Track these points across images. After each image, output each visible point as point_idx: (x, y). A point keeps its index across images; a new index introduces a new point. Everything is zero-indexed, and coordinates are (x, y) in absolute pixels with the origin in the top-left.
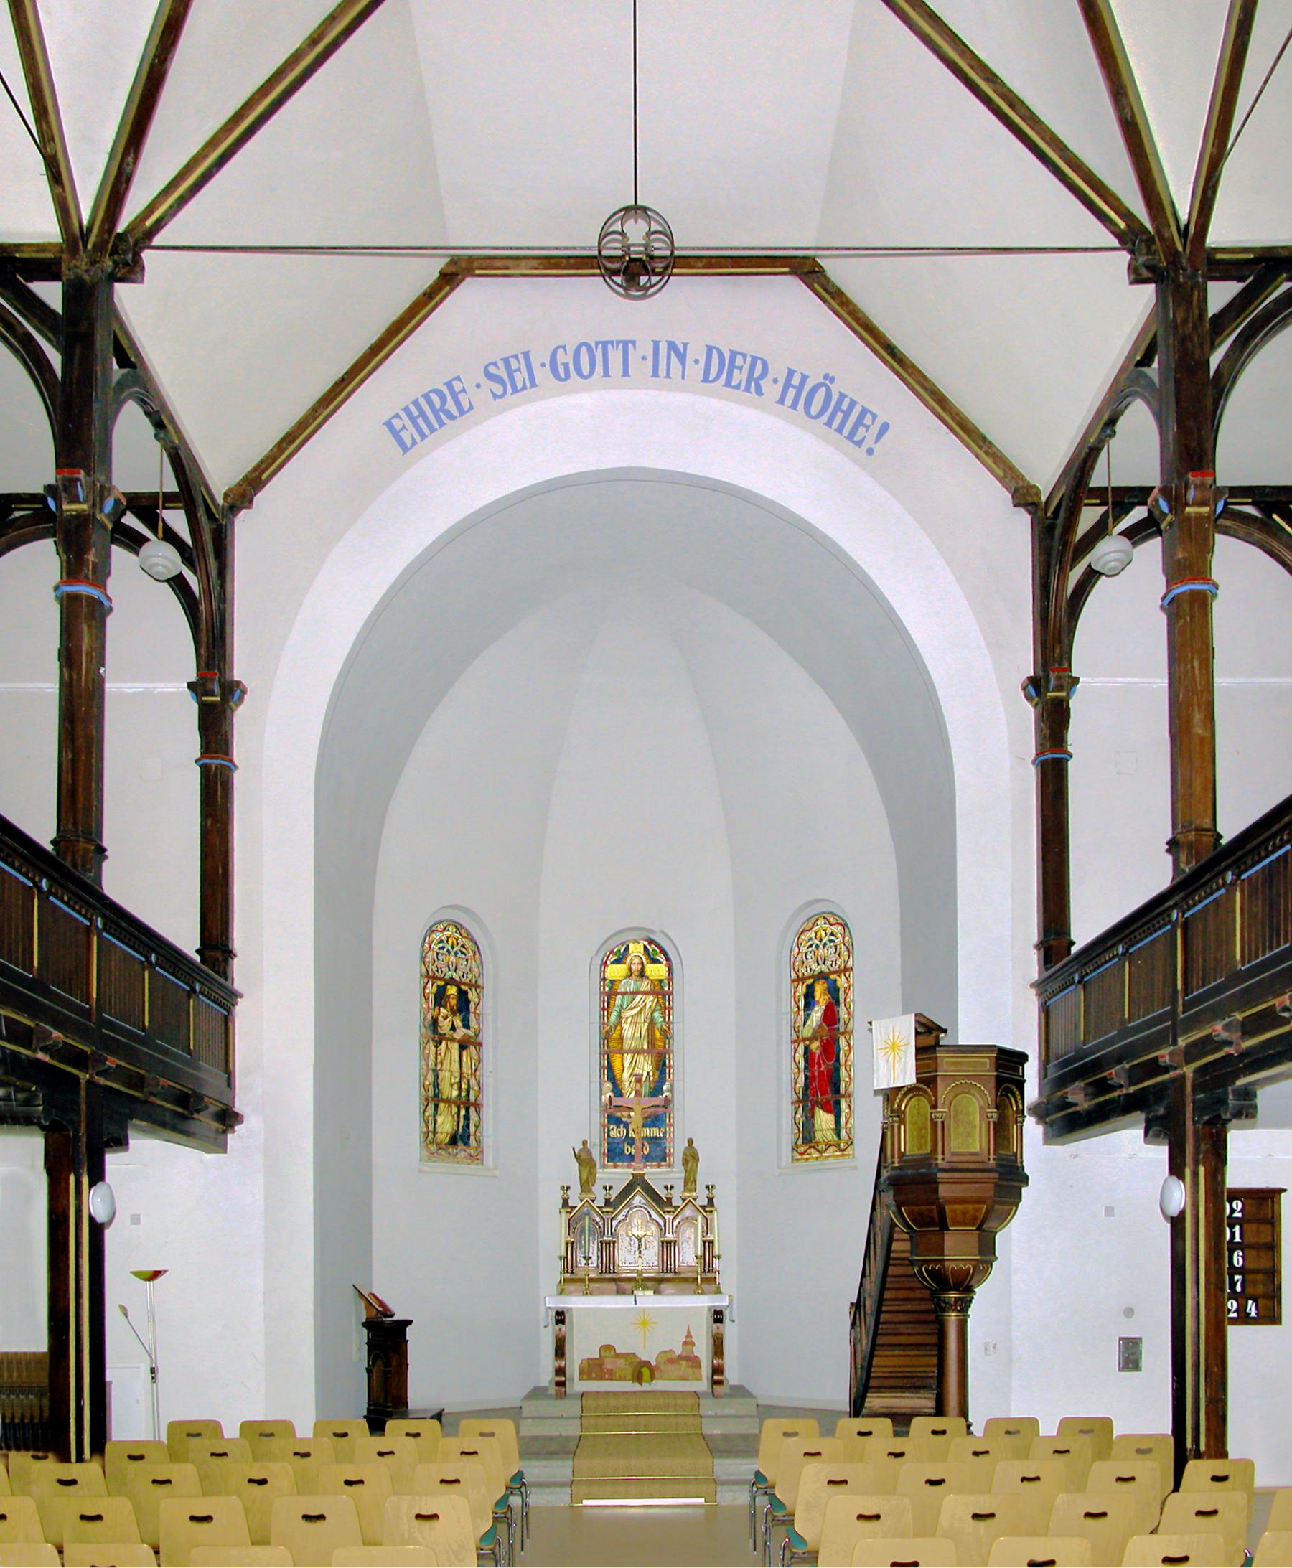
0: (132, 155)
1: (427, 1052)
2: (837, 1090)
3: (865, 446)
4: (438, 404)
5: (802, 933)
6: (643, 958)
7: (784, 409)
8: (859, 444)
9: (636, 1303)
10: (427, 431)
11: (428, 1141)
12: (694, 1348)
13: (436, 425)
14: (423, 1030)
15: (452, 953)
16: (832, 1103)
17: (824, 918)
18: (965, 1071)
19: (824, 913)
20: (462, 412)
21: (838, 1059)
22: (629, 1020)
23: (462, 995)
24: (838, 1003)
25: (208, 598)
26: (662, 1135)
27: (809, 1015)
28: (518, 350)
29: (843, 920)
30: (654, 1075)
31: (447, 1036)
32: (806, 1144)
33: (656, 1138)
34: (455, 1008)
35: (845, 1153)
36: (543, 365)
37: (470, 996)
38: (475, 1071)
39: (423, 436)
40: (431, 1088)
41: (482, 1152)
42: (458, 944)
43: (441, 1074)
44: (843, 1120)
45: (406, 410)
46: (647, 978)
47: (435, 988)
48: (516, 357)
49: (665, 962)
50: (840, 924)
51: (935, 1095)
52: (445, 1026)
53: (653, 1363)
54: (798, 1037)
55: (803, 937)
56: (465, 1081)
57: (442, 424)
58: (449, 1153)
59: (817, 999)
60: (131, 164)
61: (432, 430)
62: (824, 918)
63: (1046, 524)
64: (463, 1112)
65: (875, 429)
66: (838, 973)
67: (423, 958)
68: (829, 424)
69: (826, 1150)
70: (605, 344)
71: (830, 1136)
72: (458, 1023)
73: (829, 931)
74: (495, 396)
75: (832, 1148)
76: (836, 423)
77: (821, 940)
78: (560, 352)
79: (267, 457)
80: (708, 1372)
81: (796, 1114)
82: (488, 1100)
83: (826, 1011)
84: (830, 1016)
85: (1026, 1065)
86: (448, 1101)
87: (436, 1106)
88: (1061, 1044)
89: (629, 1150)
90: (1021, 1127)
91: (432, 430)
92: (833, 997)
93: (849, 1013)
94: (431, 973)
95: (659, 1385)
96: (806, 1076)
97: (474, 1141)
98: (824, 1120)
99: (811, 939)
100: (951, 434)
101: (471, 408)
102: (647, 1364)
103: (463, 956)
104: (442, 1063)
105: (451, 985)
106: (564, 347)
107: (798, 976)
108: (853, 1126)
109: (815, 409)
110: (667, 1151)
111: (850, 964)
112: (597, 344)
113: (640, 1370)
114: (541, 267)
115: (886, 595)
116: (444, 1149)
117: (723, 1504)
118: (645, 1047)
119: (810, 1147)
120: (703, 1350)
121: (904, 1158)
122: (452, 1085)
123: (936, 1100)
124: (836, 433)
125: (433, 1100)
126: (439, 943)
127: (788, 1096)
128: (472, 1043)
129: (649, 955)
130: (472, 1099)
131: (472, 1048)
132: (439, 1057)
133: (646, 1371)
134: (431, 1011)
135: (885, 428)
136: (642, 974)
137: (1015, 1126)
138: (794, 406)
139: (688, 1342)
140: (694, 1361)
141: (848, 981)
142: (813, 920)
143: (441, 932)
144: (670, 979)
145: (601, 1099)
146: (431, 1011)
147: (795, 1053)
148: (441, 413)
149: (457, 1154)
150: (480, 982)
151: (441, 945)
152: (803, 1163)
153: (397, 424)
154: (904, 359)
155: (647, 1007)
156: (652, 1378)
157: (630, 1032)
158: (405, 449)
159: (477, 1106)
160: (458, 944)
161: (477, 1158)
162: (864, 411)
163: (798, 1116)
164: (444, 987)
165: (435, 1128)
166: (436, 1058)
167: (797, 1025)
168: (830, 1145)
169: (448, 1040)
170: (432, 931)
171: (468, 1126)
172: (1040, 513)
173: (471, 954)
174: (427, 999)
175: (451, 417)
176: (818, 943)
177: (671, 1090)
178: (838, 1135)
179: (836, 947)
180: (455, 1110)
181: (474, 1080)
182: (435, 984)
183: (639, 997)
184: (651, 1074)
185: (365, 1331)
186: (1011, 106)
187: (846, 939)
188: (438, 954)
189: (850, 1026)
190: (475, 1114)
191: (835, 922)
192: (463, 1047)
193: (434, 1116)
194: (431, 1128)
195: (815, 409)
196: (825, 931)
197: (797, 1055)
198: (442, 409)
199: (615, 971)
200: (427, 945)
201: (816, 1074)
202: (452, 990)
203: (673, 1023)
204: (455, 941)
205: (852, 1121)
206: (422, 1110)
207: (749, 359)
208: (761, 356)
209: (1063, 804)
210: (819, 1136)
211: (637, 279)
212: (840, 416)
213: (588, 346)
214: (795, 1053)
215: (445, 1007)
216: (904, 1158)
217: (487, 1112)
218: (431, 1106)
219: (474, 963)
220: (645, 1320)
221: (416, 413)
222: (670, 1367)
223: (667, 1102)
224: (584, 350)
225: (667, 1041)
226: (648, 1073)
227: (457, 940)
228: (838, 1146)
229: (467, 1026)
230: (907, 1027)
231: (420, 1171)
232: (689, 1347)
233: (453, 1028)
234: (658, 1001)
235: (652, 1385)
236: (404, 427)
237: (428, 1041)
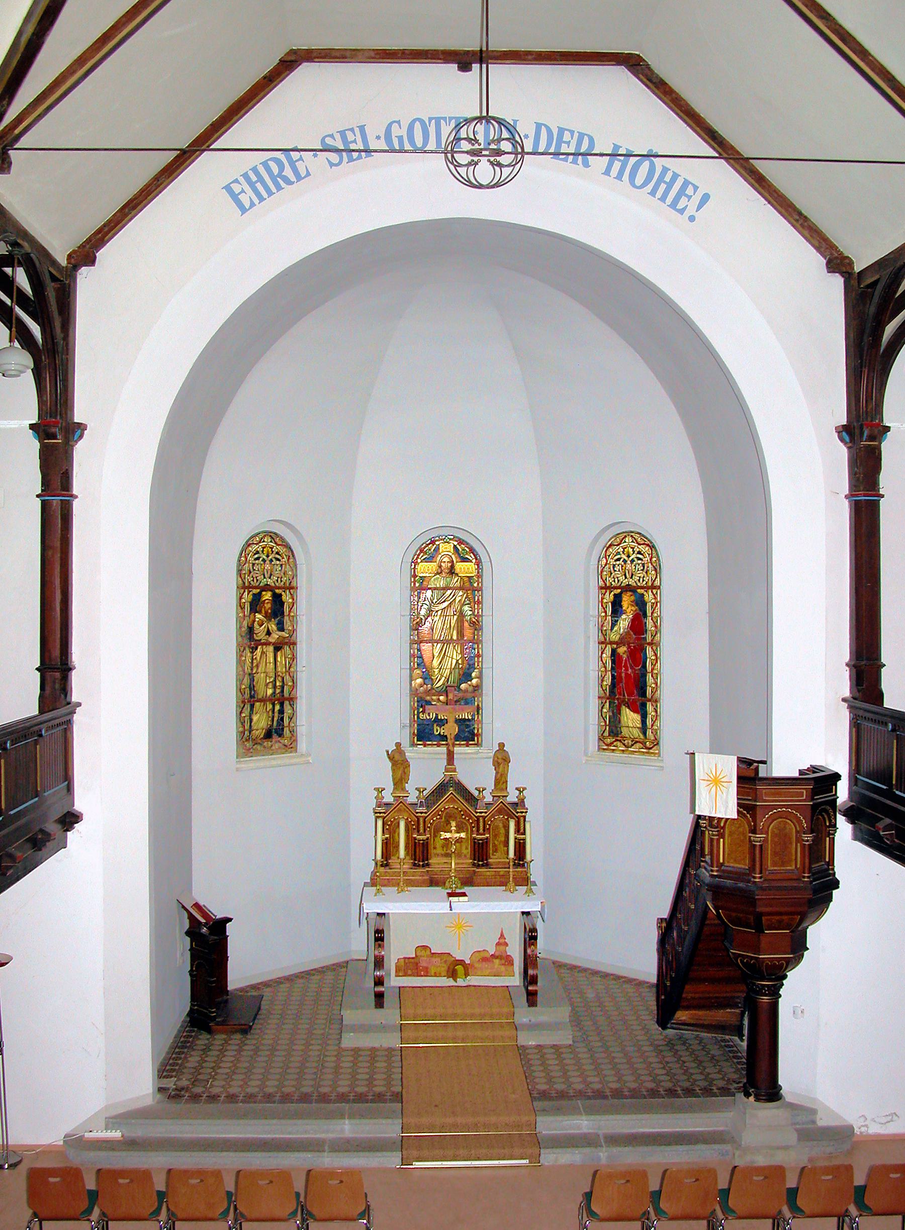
0: (7, 99)
1: (243, 658)
2: (644, 694)
3: (687, 213)
4: (275, 170)
5: (610, 545)
6: (453, 556)
7: (610, 180)
8: (682, 211)
9: (451, 910)
10: (265, 194)
11: (244, 739)
12: (507, 948)
13: (274, 190)
14: (240, 639)
15: (268, 562)
16: (638, 703)
17: (632, 536)
18: (783, 801)
19: (632, 532)
20: (299, 178)
21: (644, 666)
22: (439, 613)
23: (277, 599)
24: (645, 615)
25: (53, 379)
26: (470, 718)
27: (617, 621)
28: (354, 124)
29: (651, 543)
30: (463, 664)
31: (262, 641)
32: (613, 737)
33: (464, 720)
34: (269, 611)
35: (651, 751)
36: (378, 138)
37: (284, 598)
38: (290, 668)
39: (261, 199)
40: (247, 691)
41: (296, 740)
42: (273, 552)
43: (256, 677)
44: (649, 722)
45: (246, 176)
46: (457, 574)
47: (251, 597)
48: (352, 130)
49: (474, 561)
50: (648, 545)
51: (754, 820)
52: (260, 632)
53: (468, 962)
54: (605, 639)
55: (611, 550)
56: (280, 678)
57: (279, 188)
58: (265, 747)
59: (624, 608)
60: (6, 105)
61: (270, 193)
62: (632, 536)
63: (859, 292)
64: (277, 707)
65: (697, 199)
66: (646, 588)
67: (239, 571)
68: (653, 193)
69: (632, 745)
70: (438, 120)
71: (637, 733)
72: (273, 626)
73: (636, 549)
74: (332, 165)
75: (638, 745)
76: (659, 194)
77: (629, 556)
78: (395, 127)
79: (109, 221)
80: (520, 968)
81: (602, 708)
82: (302, 692)
83: (633, 620)
84: (638, 625)
85: (839, 783)
86: (263, 700)
87: (252, 706)
88: (870, 762)
89: (437, 730)
90: (834, 838)
91: (270, 193)
92: (640, 610)
93: (656, 627)
94: (247, 584)
95: (473, 980)
96: (613, 676)
97: (288, 732)
98: (630, 718)
99: (618, 553)
100: (769, 205)
101: (308, 174)
102: (461, 962)
103: (278, 562)
104: (257, 666)
105: (265, 591)
106: (398, 122)
107: (606, 585)
108: (659, 728)
109: (639, 181)
110: (476, 732)
111: (657, 583)
112: (430, 119)
113: (454, 968)
114: (378, 56)
115: (701, 328)
116: (259, 743)
117: (546, 1164)
118: (455, 637)
119: (617, 740)
120: (515, 950)
121: (723, 868)
122: (267, 685)
123: (755, 825)
124: (659, 201)
125: (249, 701)
126: (255, 554)
127: (594, 692)
128: (286, 643)
129: (459, 554)
130: (286, 694)
131: (287, 648)
132: (255, 661)
133: (459, 968)
134: (247, 618)
135: (705, 198)
136: (452, 571)
137: (828, 839)
138: (619, 177)
139: (502, 942)
140: (509, 961)
141: (655, 598)
142: (622, 536)
143: (257, 544)
144: (479, 576)
145: (411, 684)
146: (247, 618)
147: (602, 653)
148: (278, 179)
149: (272, 746)
150: (294, 584)
151: (256, 556)
152: (607, 753)
153: (236, 188)
154: (724, 142)
155: (457, 602)
156: (466, 974)
157: (440, 624)
158: (243, 210)
159: (292, 700)
160: (273, 552)
161: (291, 747)
162: (686, 183)
163: (605, 710)
164: (260, 594)
165: (250, 726)
166: (252, 663)
167: (605, 628)
168: (637, 742)
169: (263, 644)
170: (248, 544)
171: (282, 719)
172: (854, 283)
173: (286, 559)
174: (242, 608)
175: (289, 182)
176: (626, 558)
177: (480, 677)
178: (645, 734)
179: (643, 565)
180: (270, 706)
181: (288, 677)
182: (251, 593)
183: (449, 592)
184: (460, 662)
185: (188, 939)
186: (843, 40)
187: (654, 559)
188: (254, 564)
189: (657, 638)
190: (289, 707)
191: (643, 542)
192: (277, 648)
193: (250, 716)
194: (247, 727)
195: (639, 181)
196: (633, 548)
197: (604, 655)
198: (280, 175)
199: (425, 569)
200: (243, 559)
201: (623, 675)
202: (267, 596)
203: (482, 616)
204: (270, 550)
205: (658, 723)
206: (238, 713)
207: (576, 135)
208: (588, 133)
209: (877, 598)
210: (625, 732)
211: (469, 66)
212: (663, 187)
213: (421, 121)
214: (602, 653)
215: (260, 612)
216: (723, 868)
217: (302, 706)
218: (248, 706)
219: (288, 566)
220: (460, 922)
221: (254, 178)
222: (485, 965)
223: (477, 688)
224: (417, 125)
225: (476, 632)
226: (457, 661)
227: (272, 548)
228: (644, 743)
229: (281, 628)
230: (729, 767)
231: (237, 770)
232: (502, 948)
233: (269, 633)
234: (467, 596)
235: (466, 981)
236: (243, 191)
237: (244, 649)
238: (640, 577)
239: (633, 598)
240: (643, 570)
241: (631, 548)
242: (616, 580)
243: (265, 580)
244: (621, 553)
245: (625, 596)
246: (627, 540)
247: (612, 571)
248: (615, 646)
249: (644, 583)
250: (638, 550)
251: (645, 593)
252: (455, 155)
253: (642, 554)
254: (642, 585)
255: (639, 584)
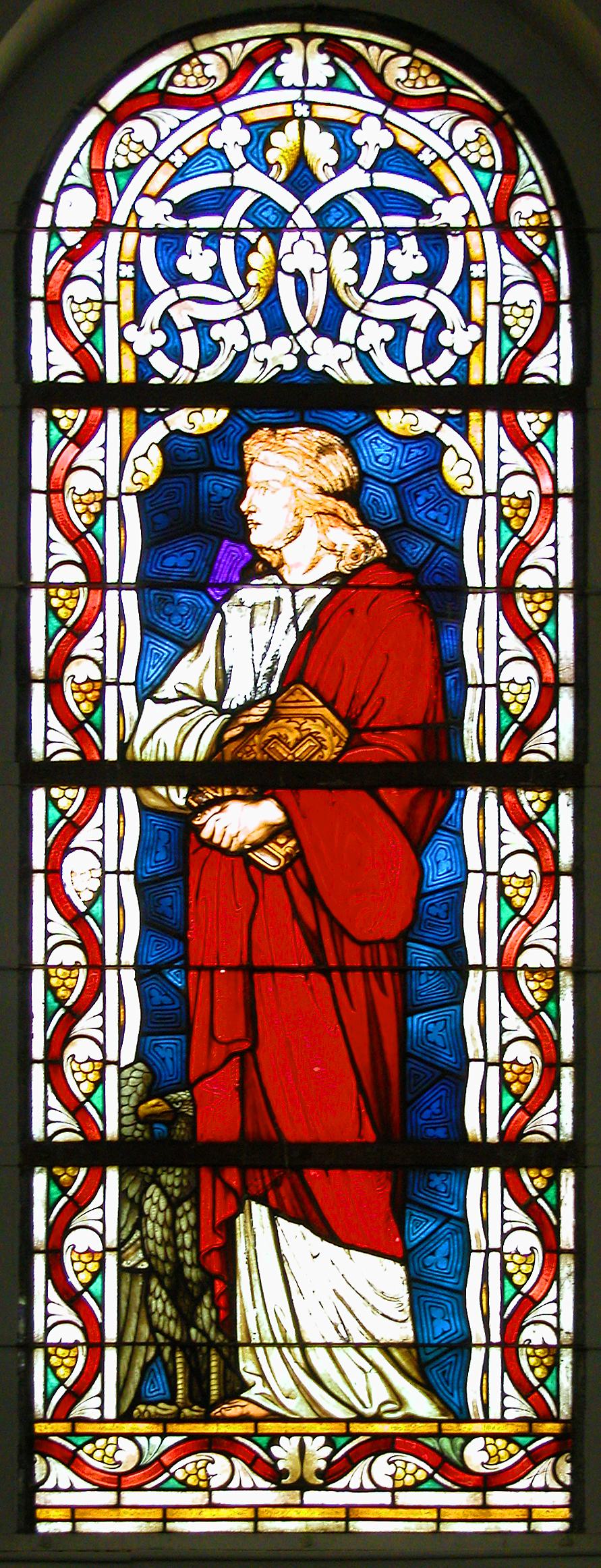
73: (372, 137)
238: (403, 326)
239: (338, 467)
240: (429, 279)
241: (325, 124)
242: (190, 342)
243: (282, 343)
244: (236, 158)
245: (272, 457)
246: (290, 67)
247: (155, 281)
248: (178, 796)
249: (445, 362)
250: (386, 141)
251: (448, 435)
252: (550, 586)
253: (424, 174)
254: (421, 378)
255: (397, 374)
